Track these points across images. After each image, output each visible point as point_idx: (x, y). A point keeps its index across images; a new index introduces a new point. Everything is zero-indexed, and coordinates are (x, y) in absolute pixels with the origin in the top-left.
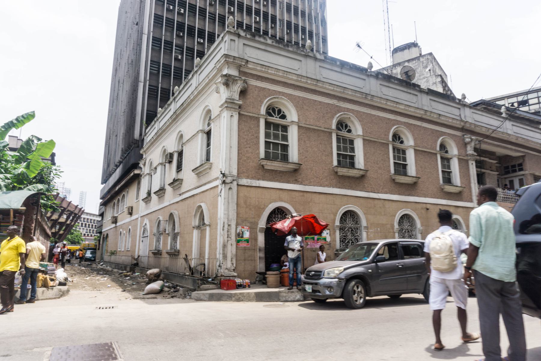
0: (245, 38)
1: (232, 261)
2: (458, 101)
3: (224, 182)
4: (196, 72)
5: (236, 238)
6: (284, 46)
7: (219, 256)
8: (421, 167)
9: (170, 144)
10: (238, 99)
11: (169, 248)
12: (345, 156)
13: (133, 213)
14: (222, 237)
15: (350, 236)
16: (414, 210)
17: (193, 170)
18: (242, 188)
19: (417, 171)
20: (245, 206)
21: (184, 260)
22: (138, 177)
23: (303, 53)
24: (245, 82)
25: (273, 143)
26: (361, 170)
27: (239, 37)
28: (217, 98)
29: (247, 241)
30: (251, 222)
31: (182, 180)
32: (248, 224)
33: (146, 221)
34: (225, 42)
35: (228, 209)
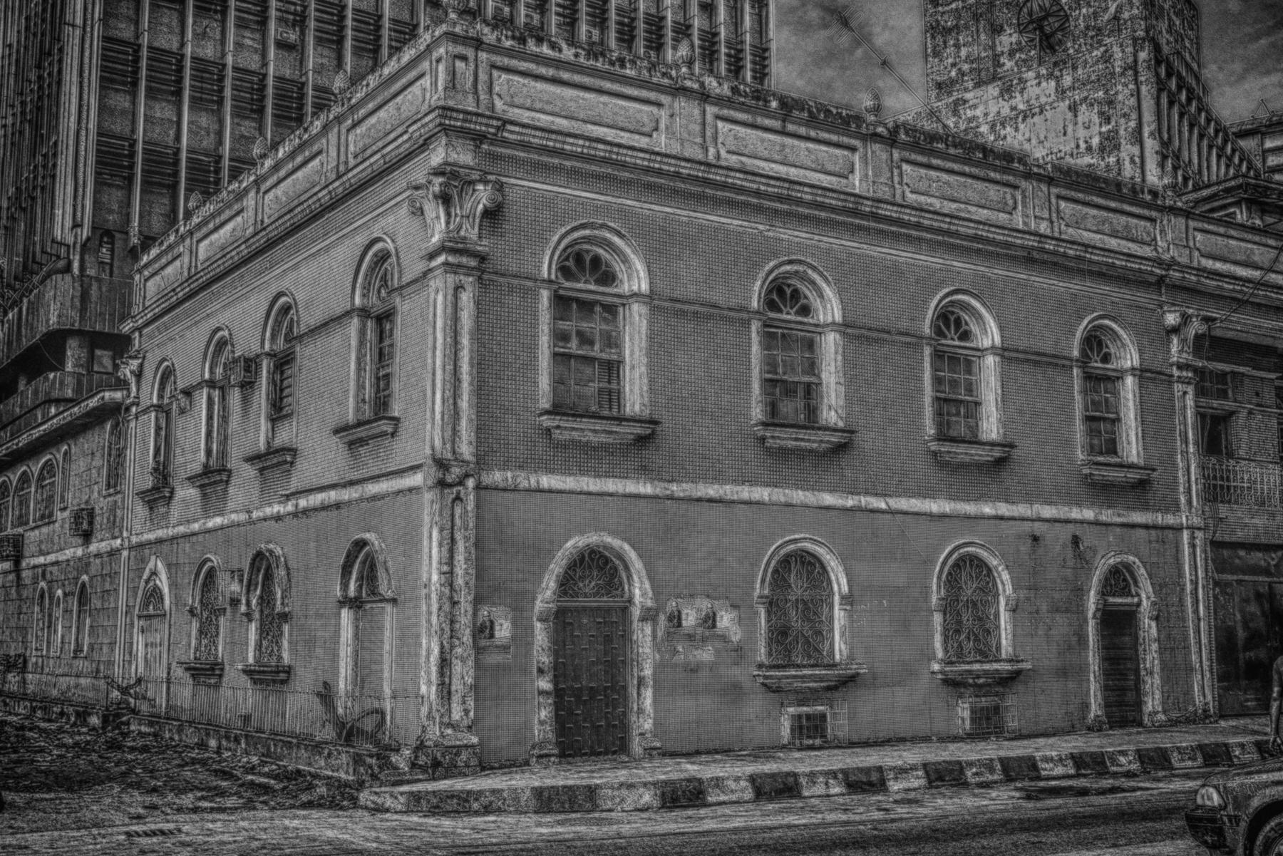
0: (495, 49)
2: (1148, 197)
3: (442, 484)
6: (612, 63)
8: (1021, 412)
11: (251, 660)
19: (1005, 423)
21: (317, 700)
23: (666, 81)
24: (500, 187)
28: (413, 228)
29: (505, 648)
31: (293, 451)
35: (452, 557)
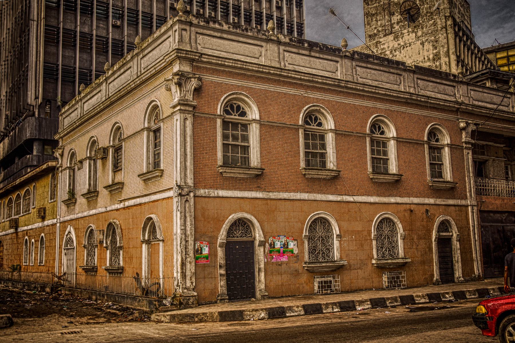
0: (198, 26)
1: (191, 279)
4: (137, 55)
5: (195, 255)
6: (243, 30)
7: (177, 275)
9: (102, 133)
10: (191, 99)
12: (314, 155)
13: (47, 217)
14: (180, 255)
15: (320, 246)
16: (396, 213)
17: (139, 176)
18: (200, 199)
19: (399, 166)
20: (203, 219)
22: (52, 171)
23: (264, 37)
24: (200, 79)
25: (231, 145)
26: (333, 170)
27: (190, 26)
28: (167, 96)
29: (207, 258)
30: (210, 237)
31: (122, 184)
32: (207, 239)
33: (70, 229)
34: (175, 31)
